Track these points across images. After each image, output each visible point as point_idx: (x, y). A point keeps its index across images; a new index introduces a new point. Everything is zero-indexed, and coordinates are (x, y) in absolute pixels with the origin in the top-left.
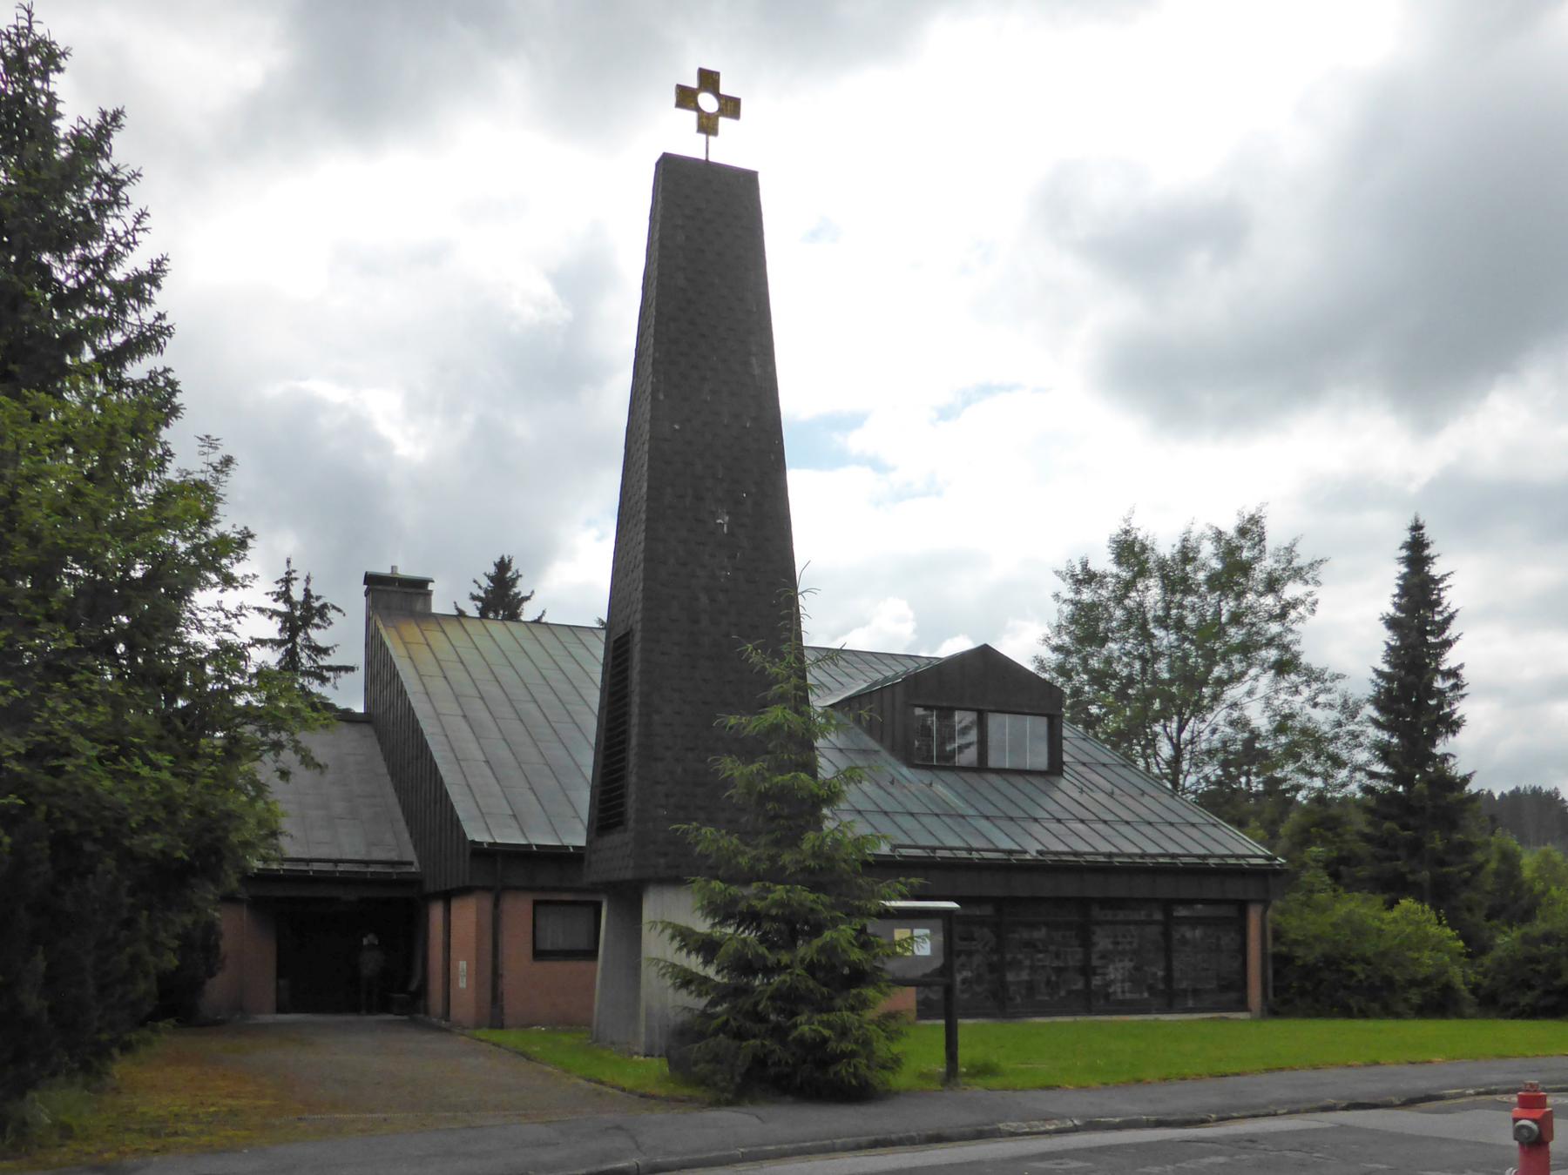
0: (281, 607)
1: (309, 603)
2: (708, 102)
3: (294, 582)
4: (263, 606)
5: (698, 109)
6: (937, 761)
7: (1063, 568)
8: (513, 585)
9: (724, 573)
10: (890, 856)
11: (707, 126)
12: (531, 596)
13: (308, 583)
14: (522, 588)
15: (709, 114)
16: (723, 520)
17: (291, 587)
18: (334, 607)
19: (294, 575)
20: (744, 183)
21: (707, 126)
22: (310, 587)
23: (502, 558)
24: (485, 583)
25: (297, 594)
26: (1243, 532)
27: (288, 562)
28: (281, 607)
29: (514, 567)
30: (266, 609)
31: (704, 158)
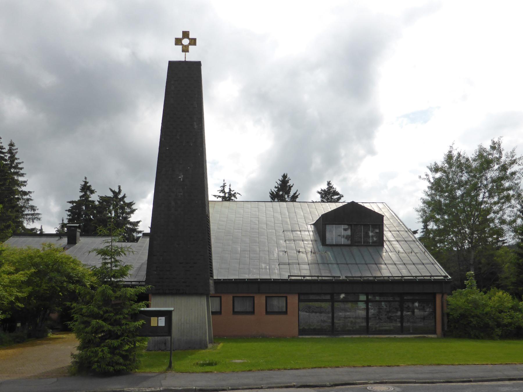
0: (222, 194)
1: (231, 192)
2: (186, 42)
3: (225, 187)
4: (216, 195)
5: (182, 44)
6: (363, 243)
7: (429, 165)
8: (288, 182)
9: (180, 194)
10: (317, 280)
11: (185, 50)
12: (293, 185)
13: (230, 186)
14: (290, 183)
15: (185, 45)
16: (181, 177)
17: (225, 188)
18: (238, 193)
19: (225, 184)
20: (197, 65)
21: (185, 50)
22: (230, 188)
23: (284, 174)
24: (279, 182)
25: (227, 190)
26: (493, 148)
27: (224, 181)
28: (222, 194)
29: (288, 176)
30: (217, 196)
31: (184, 60)
